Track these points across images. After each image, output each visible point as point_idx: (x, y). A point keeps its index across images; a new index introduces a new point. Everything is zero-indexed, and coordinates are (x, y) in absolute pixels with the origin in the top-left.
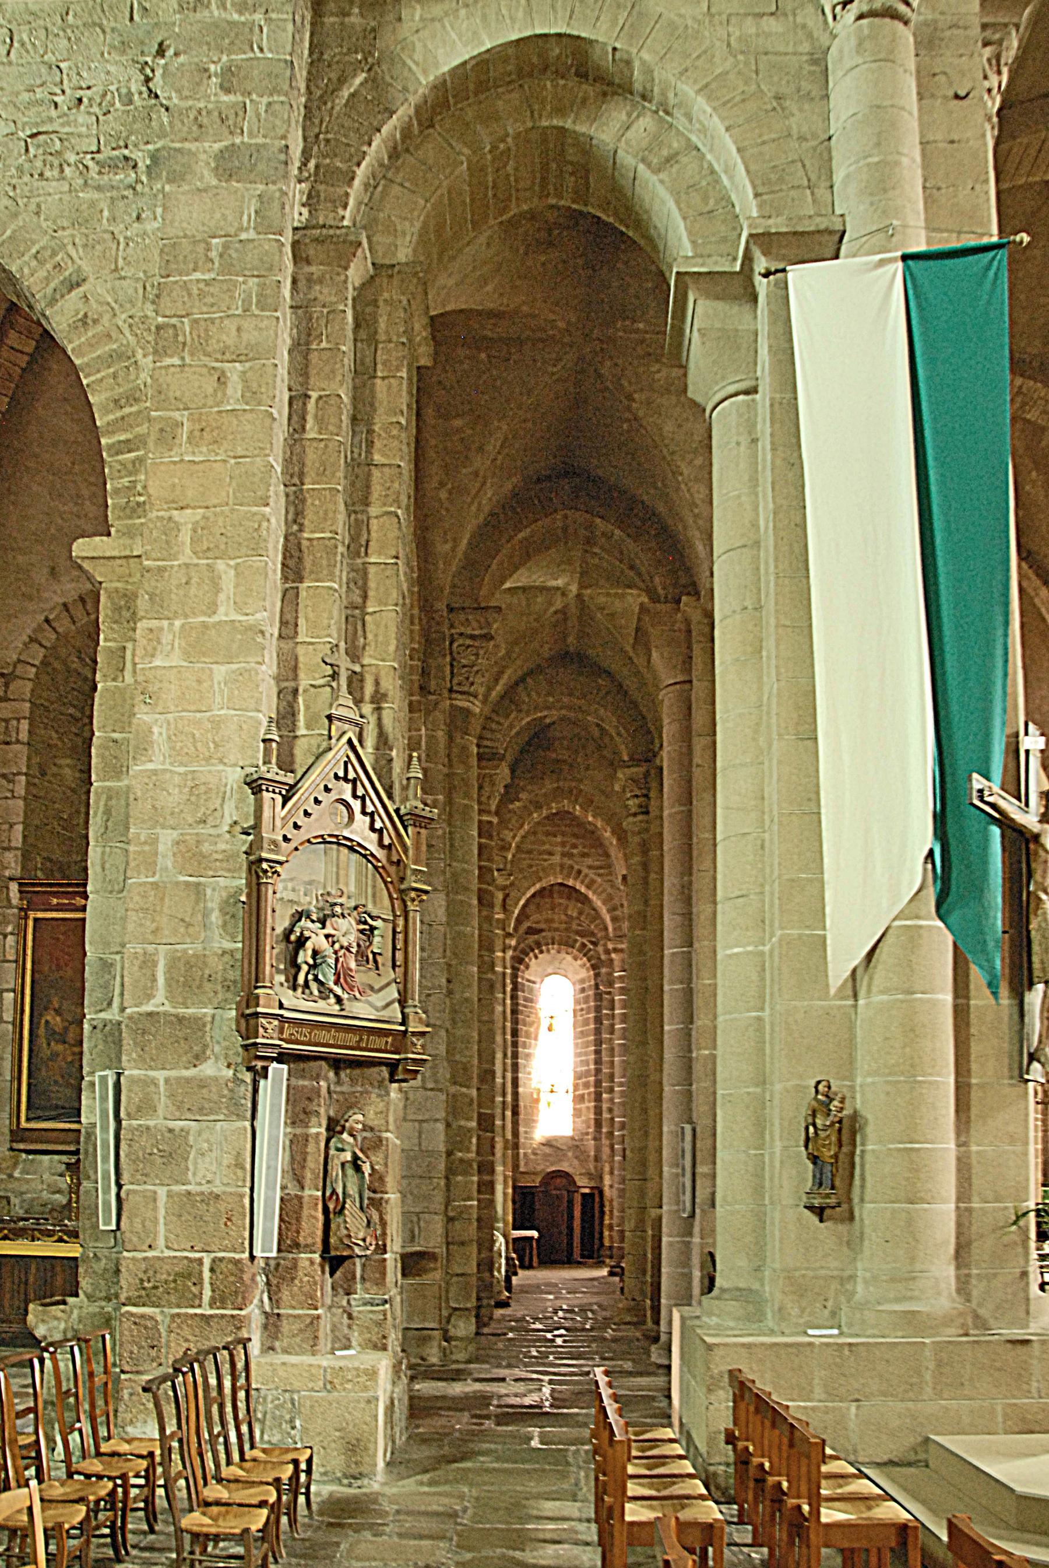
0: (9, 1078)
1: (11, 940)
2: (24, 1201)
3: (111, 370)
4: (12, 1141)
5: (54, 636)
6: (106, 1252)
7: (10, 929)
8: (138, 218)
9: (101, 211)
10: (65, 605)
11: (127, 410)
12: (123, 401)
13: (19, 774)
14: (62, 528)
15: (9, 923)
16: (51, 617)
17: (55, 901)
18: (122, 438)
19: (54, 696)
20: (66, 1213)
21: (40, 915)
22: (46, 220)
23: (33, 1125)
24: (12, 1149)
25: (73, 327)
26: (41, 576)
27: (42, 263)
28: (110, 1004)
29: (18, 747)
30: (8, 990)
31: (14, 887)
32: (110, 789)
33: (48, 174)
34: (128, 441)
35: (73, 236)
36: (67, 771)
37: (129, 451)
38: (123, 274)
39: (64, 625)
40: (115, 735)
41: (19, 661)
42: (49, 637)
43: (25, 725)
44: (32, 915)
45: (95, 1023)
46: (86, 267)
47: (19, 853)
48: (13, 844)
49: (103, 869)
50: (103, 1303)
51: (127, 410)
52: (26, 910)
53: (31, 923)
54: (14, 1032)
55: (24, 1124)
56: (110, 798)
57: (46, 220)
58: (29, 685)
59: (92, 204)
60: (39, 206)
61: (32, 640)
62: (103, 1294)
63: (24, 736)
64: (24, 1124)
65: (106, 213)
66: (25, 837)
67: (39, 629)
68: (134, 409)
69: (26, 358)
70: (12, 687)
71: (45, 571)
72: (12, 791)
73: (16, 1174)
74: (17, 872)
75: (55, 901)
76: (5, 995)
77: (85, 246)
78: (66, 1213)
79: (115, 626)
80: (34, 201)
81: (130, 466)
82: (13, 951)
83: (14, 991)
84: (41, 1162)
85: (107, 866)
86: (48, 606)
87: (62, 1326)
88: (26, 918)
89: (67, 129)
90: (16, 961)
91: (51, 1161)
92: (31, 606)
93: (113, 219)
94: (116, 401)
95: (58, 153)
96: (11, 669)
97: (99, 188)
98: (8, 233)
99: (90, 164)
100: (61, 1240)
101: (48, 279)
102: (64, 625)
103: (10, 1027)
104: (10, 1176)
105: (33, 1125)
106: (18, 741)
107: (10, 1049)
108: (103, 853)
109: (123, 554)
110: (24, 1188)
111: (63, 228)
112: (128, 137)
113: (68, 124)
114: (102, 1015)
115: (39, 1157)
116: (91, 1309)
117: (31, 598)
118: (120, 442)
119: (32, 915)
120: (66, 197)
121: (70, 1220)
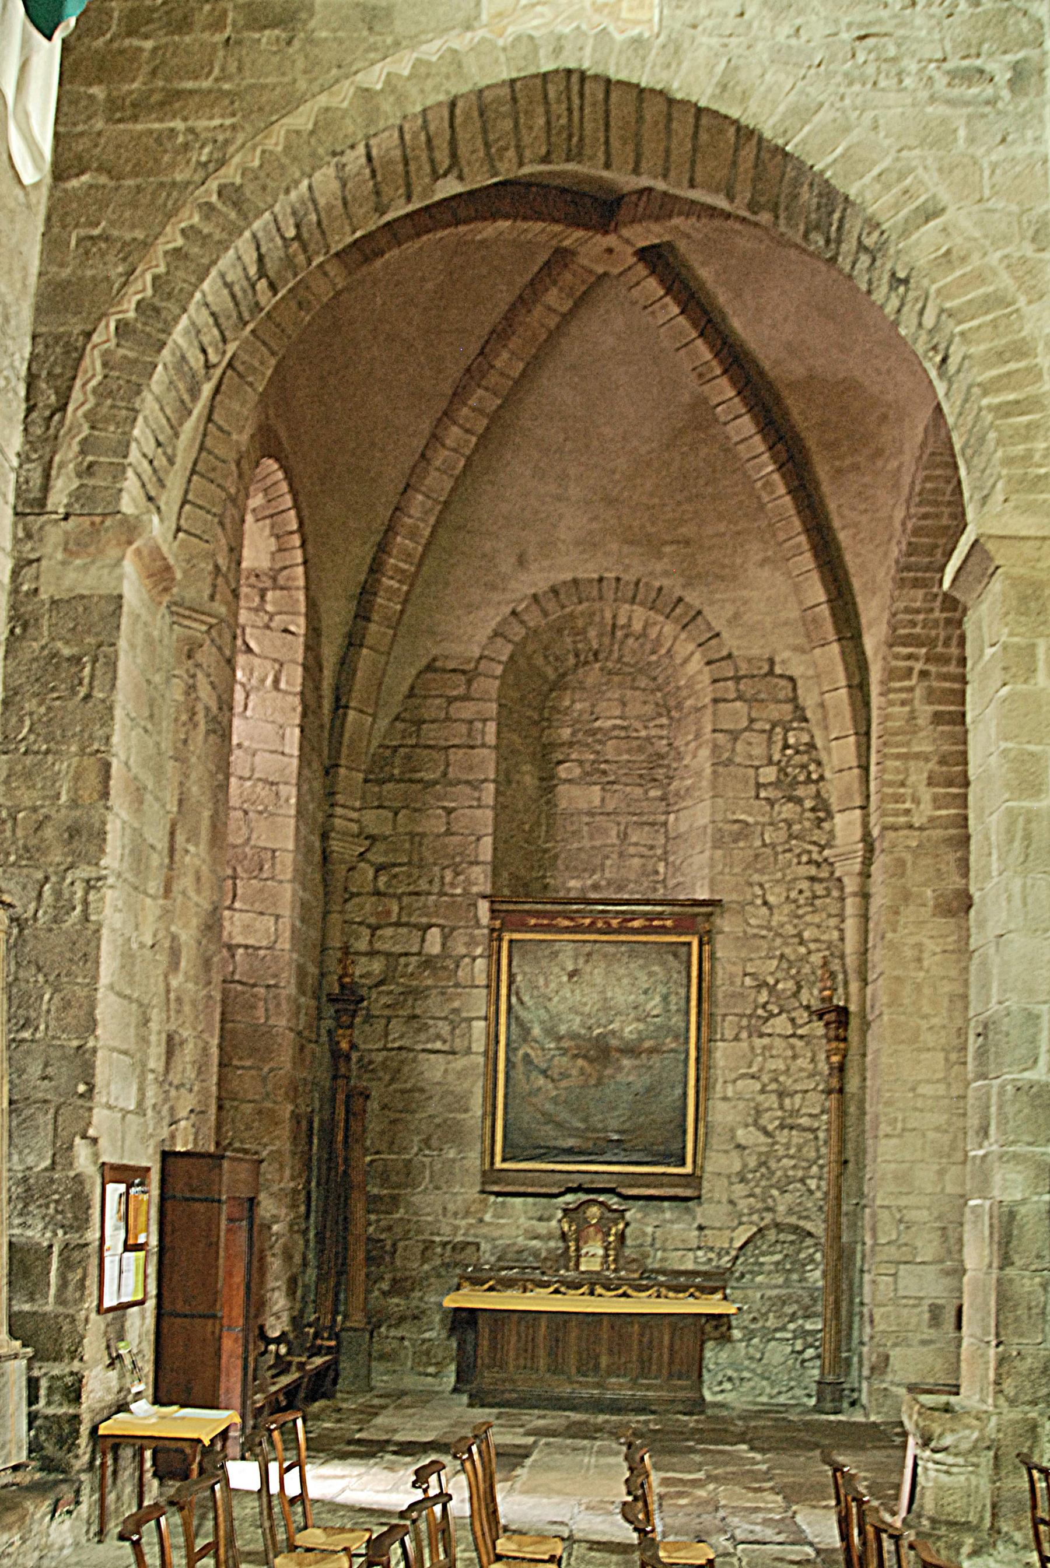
0: (479, 1113)
1: (481, 963)
2: (495, 1247)
3: (989, 317)
4: (483, 1183)
5: (523, 631)
6: (1031, 1350)
7: (479, 951)
8: (1003, 140)
9: (955, 131)
10: (535, 596)
11: (1012, 366)
12: (1007, 355)
13: (485, 780)
14: (537, 512)
15: (478, 945)
16: (519, 609)
17: (533, 922)
18: (1012, 397)
19: (517, 695)
20: (562, 1262)
21: (516, 936)
22: (886, 136)
23: (506, 1166)
24: (483, 1192)
25: (936, 262)
26: (506, 564)
27: (888, 187)
28: (1035, 1061)
29: (486, 751)
30: (478, 1018)
31: (484, 906)
32: (1029, 811)
33: (883, 84)
34: (1017, 402)
35: (923, 159)
36: (528, 779)
37: (1022, 414)
38: (990, 205)
39: (533, 619)
40: (1031, 748)
41: (481, 658)
42: (518, 632)
43: (492, 727)
44: (507, 936)
45: (1019, 1084)
46: (945, 197)
47: (489, 868)
48: (481, 858)
49: (1025, 904)
50: (1027, 1408)
51: (1012, 366)
52: (501, 930)
53: (505, 945)
54: (486, 1065)
55: (499, 1165)
56: (1028, 821)
57: (886, 136)
58: (497, 683)
59: (944, 121)
60: (875, 120)
61: (496, 634)
62: (1028, 1398)
63: (491, 739)
64: (499, 1165)
65: (962, 133)
66: (495, 849)
67: (504, 621)
68: (1022, 364)
69: (557, 319)
70: (475, 685)
71: (513, 560)
72: (479, 799)
73: (488, 1218)
74: (488, 890)
75: (533, 922)
76: (475, 1023)
77: (940, 170)
78: (562, 1262)
79: (1023, 619)
80: (869, 115)
81: (1023, 431)
82: (484, 976)
83: (486, 1019)
84: (513, 1206)
85: (1030, 900)
86: (518, 595)
87: (976, 1435)
88: (500, 939)
89: (901, 32)
90: (488, 986)
91: (525, 1204)
92: (496, 597)
93: (971, 140)
94: (1000, 354)
95: (894, 60)
96: (472, 665)
97: (950, 102)
98: (839, 151)
99: (937, 75)
100: (557, 1291)
101: (897, 206)
102: (533, 619)
103: (481, 1060)
104: (481, 1220)
105: (506, 1166)
106: (483, 745)
107: (480, 1083)
108: (1024, 886)
109: (1040, 534)
110: (497, 1233)
111: (910, 149)
112: (980, 44)
113: (901, 25)
114: (1026, 1075)
115: (509, 1199)
116: (1012, 1416)
117: (493, 587)
118: (1008, 403)
119: (507, 936)
120: (909, 111)
121: (567, 1269)
